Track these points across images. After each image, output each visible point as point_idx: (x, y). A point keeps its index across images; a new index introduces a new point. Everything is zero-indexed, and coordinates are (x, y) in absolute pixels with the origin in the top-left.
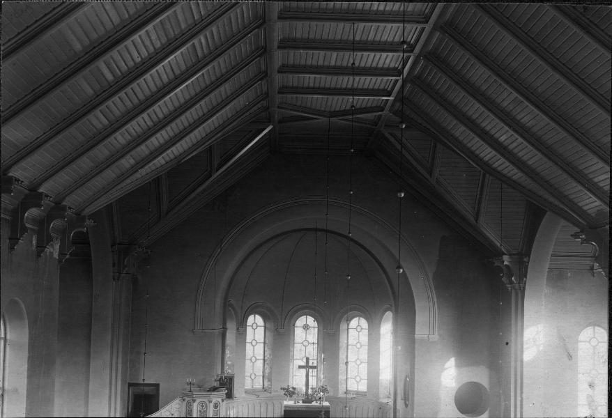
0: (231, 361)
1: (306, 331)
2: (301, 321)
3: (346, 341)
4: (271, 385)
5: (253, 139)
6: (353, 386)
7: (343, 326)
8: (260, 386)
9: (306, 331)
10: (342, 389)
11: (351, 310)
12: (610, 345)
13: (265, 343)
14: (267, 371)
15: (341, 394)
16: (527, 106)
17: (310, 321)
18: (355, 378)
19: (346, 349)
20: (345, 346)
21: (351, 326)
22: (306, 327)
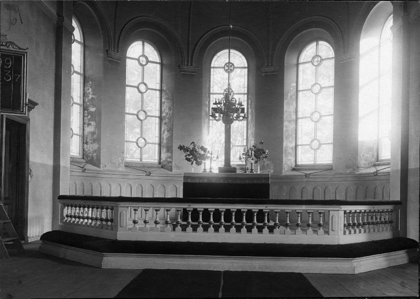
0: (94, 106)
1: (229, 73)
2: (220, 59)
3: (295, 84)
4: (171, 157)
5: (229, 275)
6: (305, 158)
7: (290, 59)
8: (154, 159)
9: (229, 73)
10: (288, 162)
11: (298, 30)
12: (419, 194)
13: (161, 91)
14: (166, 135)
15: (286, 171)
16: (261, 211)
17: (238, 59)
18: (310, 141)
19: (294, 97)
20: (293, 91)
21: (301, 60)
22: (229, 67)
